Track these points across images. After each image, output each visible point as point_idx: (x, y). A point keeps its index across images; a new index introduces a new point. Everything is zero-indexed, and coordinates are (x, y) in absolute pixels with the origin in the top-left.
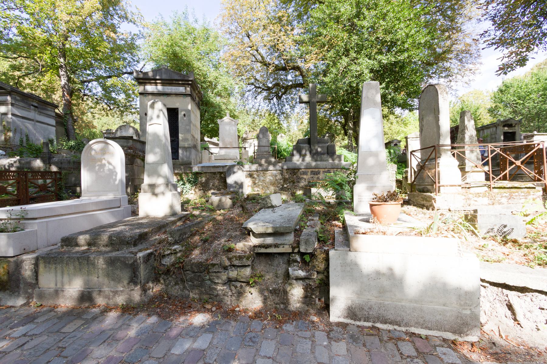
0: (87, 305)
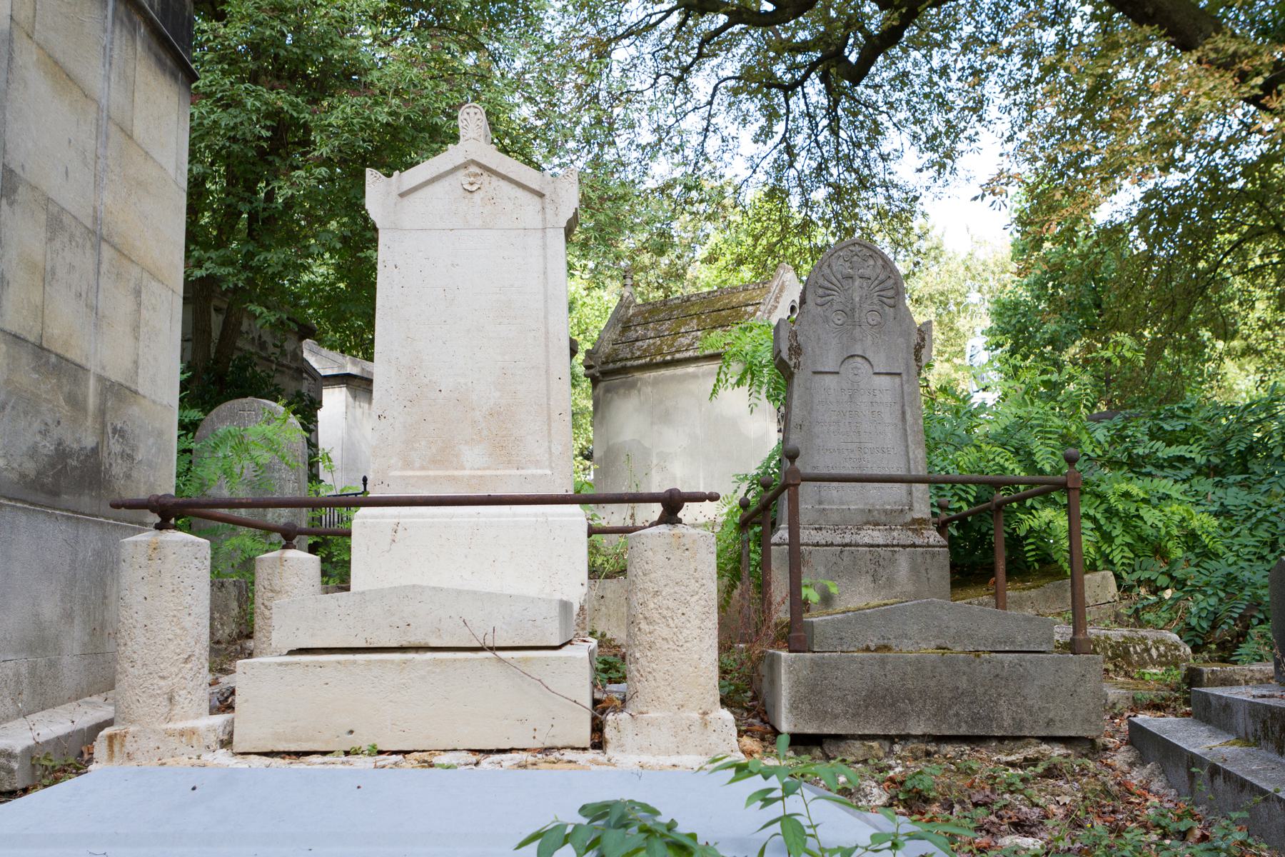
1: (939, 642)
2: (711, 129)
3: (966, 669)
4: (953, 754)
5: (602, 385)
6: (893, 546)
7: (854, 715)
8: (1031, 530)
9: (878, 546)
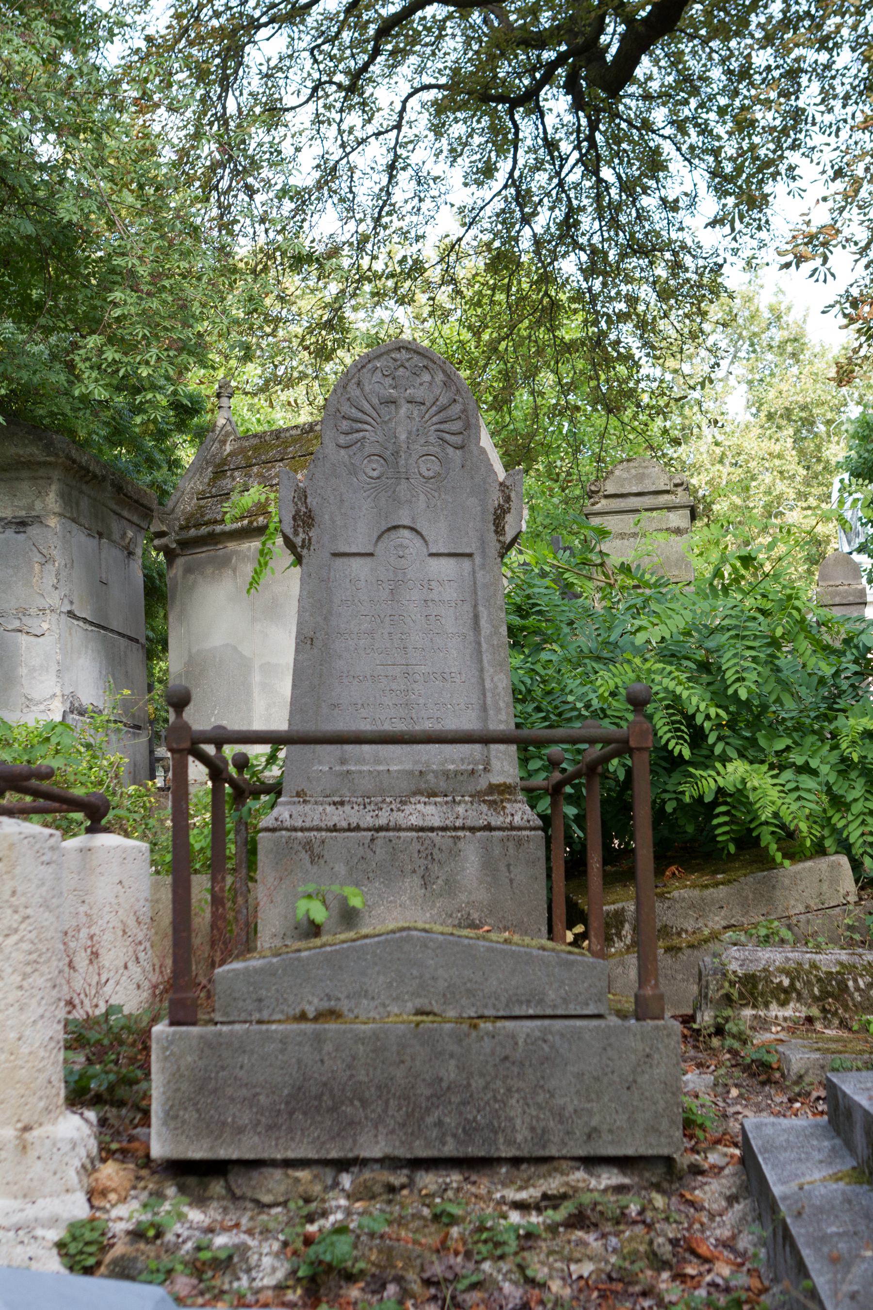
0: (220, 1240)
1: (419, 1002)
2: (400, 164)
3: (453, 1047)
4: (433, 1188)
5: (180, 561)
6: (456, 829)
7: (269, 1128)
8: (720, 791)
9: (432, 829)
